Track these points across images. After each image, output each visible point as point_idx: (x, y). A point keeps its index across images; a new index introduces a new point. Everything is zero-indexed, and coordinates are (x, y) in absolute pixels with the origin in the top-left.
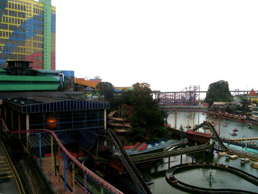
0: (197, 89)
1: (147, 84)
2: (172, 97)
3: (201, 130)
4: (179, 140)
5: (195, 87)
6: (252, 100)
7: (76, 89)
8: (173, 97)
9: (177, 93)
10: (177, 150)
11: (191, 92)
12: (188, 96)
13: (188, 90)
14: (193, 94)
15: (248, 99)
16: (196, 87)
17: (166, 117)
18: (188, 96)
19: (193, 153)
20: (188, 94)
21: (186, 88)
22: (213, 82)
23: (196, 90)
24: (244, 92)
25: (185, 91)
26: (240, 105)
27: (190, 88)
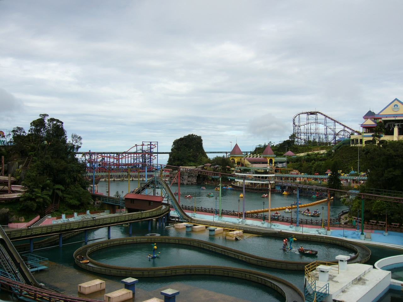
0: (154, 147)
1: (58, 121)
5: (151, 145)
6: (236, 160)
11: (143, 153)
16: (152, 143)
21: (136, 145)
23: (153, 148)
25: (134, 150)
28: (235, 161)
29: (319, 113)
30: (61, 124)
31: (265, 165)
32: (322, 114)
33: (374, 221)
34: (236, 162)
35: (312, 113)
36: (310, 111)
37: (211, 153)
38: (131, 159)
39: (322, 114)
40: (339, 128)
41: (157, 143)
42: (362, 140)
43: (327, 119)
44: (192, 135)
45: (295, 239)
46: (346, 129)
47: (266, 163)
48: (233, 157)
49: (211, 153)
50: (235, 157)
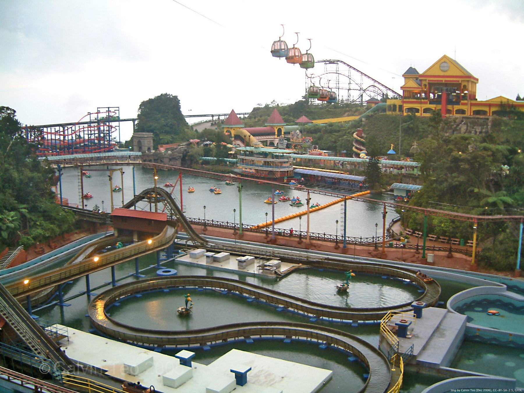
2: (58, 137)
3: (142, 206)
4: (95, 232)
5: (109, 111)
6: (233, 133)
7: (162, 132)
8: (60, 135)
9: (69, 126)
10: (62, 268)
12: (94, 131)
13: (93, 117)
14: (105, 127)
15: (225, 131)
17: (56, 181)
18: (94, 131)
19: (136, 259)
20: (94, 127)
21: (90, 114)
22: (146, 99)
24: (213, 116)
25: (87, 119)
26: (210, 144)
27: (98, 112)
28: (231, 134)
29: (342, 62)
30: (13, 112)
31: (272, 137)
32: (345, 63)
33: (433, 236)
34: (233, 136)
35: (331, 62)
36: (328, 59)
37: (191, 116)
38: (84, 134)
39: (345, 63)
40: (367, 83)
41: (117, 109)
42: (401, 106)
43: (352, 70)
44: (166, 94)
45: (353, 274)
46: (376, 84)
47: (274, 134)
48: (228, 128)
49: (191, 116)
50: (232, 128)
